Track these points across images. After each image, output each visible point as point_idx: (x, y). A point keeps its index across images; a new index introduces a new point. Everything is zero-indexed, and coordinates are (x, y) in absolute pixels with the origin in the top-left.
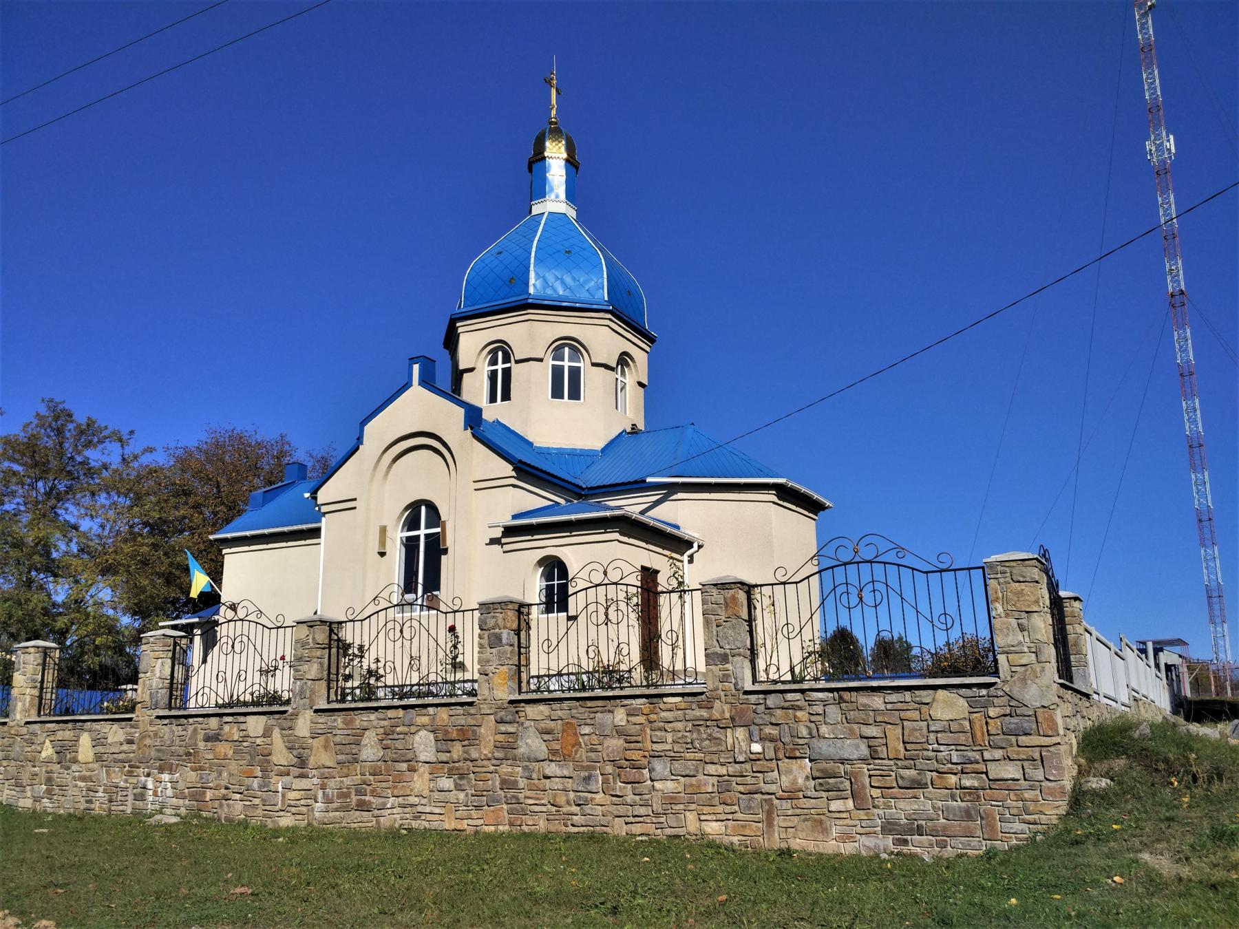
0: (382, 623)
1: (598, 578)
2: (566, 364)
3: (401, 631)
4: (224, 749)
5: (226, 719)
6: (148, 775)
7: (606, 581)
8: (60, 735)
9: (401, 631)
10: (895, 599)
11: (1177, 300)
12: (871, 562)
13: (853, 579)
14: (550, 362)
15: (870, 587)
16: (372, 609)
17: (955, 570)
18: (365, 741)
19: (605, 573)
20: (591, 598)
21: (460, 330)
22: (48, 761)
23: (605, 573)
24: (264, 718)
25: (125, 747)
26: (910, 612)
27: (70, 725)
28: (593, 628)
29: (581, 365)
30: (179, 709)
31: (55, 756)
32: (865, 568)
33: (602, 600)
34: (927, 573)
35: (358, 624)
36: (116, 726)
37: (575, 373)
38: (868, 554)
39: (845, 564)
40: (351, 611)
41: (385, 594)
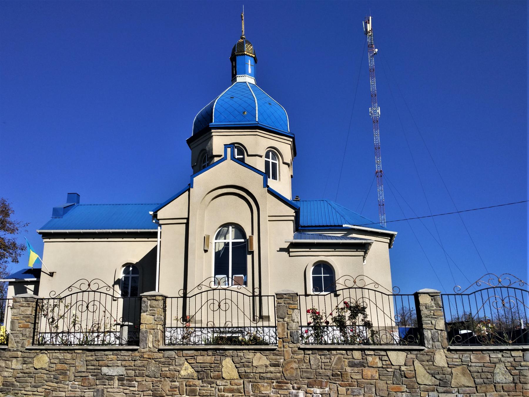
0: (204, 300)
1: (85, 287)
2: (271, 160)
3: (87, 307)
4: (368, 372)
5: (368, 352)
6: (299, 389)
7: (89, 290)
8: (200, 359)
9: (87, 307)
10: (235, 307)
11: (379, 174)
12: (362, 288)
13: (86, 299)
14: (264, 159)
15: (224, 301)
16: (67, 293)
17: (401, 295)
18: (497, 370)
19: (89, 285)
20: (80, 298)
21: (213, 134)
22: (189, 378)
23: (89, 285)
24: (404, 354)
25: (272, 369)
26: (380, 313)
27: (210, 353)
28: (211, 313)
29: (277, 162)
30: (350, 344)
31: (195, 374)
32: (92, 294)
33: (86, 299)
34: (388, 295)
35: (472, 297)
36: (258, 354)
37: (274, 165)
38: (94, 287)
39: (349, 288)
40: (53, 293)
41: (77, 285)
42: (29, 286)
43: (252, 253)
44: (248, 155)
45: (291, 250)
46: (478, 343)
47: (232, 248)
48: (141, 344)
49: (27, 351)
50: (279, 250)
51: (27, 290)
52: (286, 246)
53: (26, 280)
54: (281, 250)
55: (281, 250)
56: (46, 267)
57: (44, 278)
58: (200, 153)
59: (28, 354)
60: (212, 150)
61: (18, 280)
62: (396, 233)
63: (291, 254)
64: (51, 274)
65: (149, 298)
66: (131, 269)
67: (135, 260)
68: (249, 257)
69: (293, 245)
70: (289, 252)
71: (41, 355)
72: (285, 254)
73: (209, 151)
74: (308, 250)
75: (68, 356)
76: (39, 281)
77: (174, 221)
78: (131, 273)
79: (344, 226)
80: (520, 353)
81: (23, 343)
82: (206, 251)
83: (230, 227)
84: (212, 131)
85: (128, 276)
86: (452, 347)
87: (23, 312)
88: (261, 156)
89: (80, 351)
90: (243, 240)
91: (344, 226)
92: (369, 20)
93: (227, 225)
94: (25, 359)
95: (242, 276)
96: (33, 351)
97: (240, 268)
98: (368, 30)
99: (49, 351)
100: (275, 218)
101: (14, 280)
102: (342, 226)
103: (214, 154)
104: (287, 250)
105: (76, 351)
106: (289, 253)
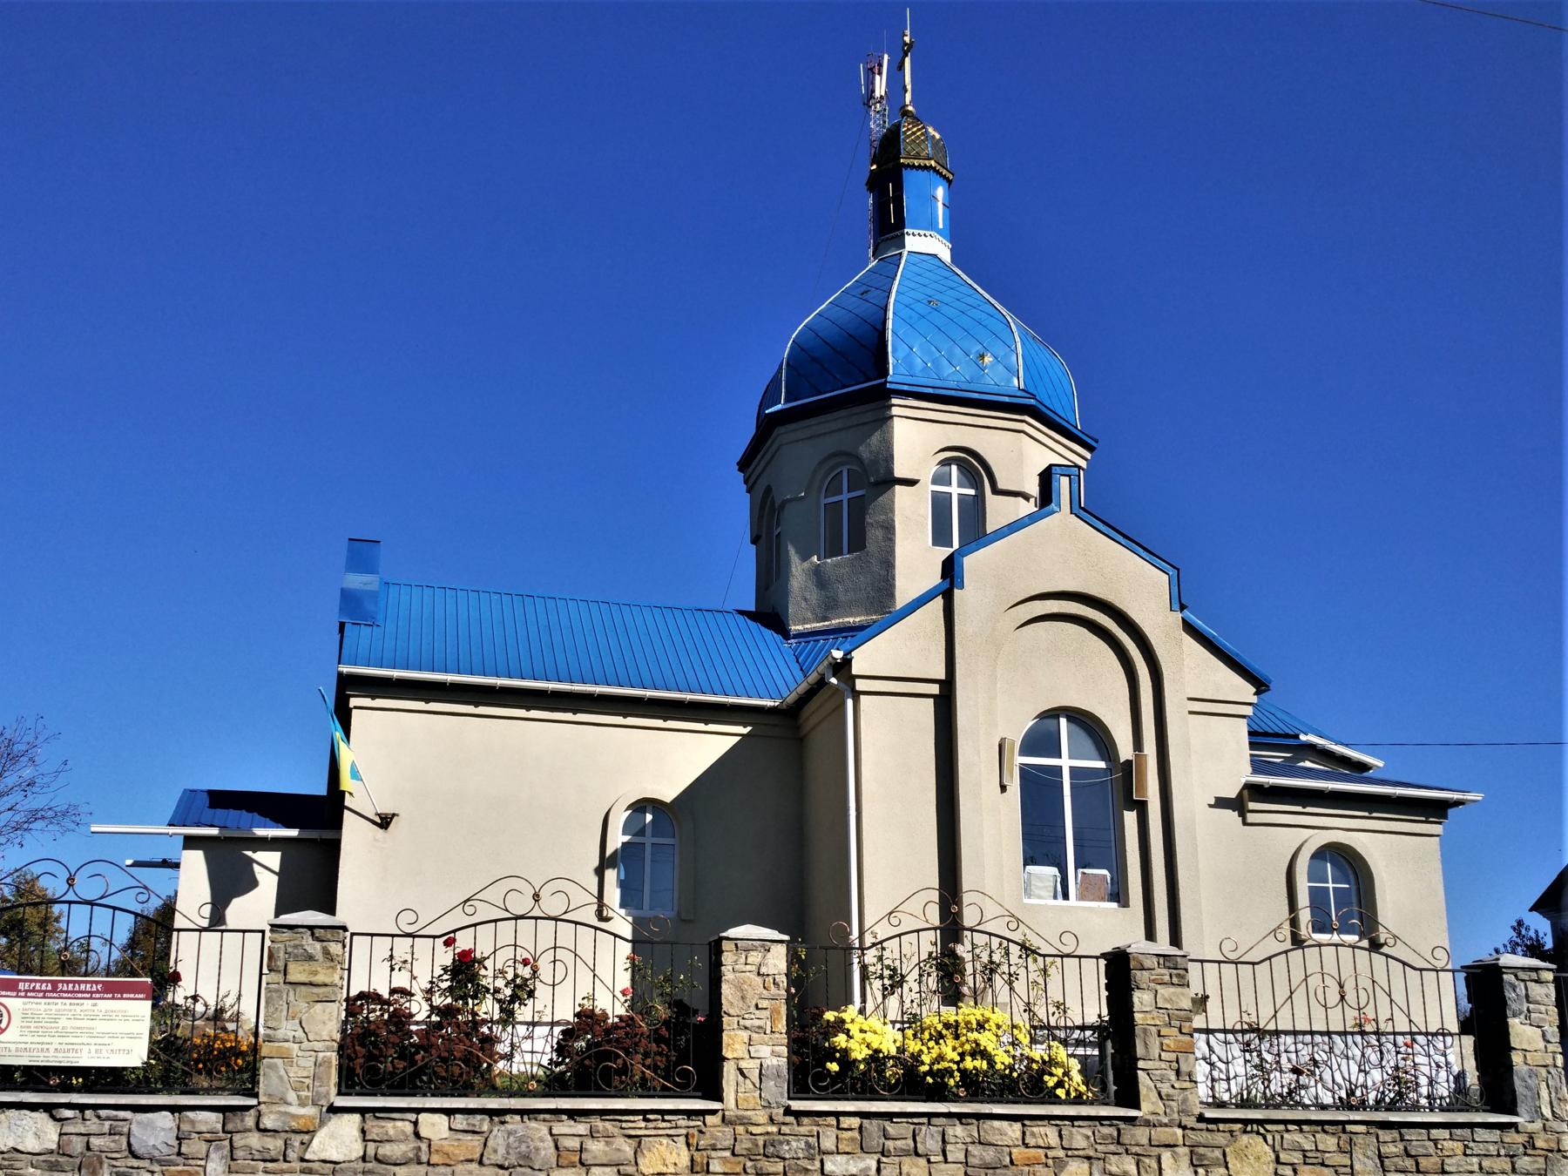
21: (895, 411)
42: (260, 856)
43: (1141, 808)
44: (996, 491)
45: (1252, 805)
46: (873, 1091)
47: (1072, 784)
48: (1521, 1108)
49: (1203, 1126)
50: (1212, 802)
51: (256, 868)
52: (1232, 793)
53: (260, 832)
54: (1221, 803)
55: (1221, 803)
56: (360, 796)
57: (354, 835)
58: (821, 463)
59: (1205, 1134)
60: (889, 459)
61: (228, 834)
62: (1380, 764)
63: (1251, 818)
64: (384, 822)
65: (1521, 975)
66: (649, 817)
67: (668, 792)
68: (1130, 818)
69: (1255, 792)
70: (1243, 812)
71: (1245, 1138)
72: (1232, 816)
73: (875, 462)
74: (1299, 809)
75: (1329, 1142)
76: (339, 841)
77: (900, 685)
78: (649, 831)
79: (1303, 737)
80: (214, 1119)
81: (1185, 1101)
82: (1003, 788)
83: (1063, 721)
84: (894, 401)
85: (639, 840)
86: (797, 1105)
87: (1166, 1000)
88: (1027, 497)
89: (1362, 1128)
90: (1102, 765)
91: (1303, 737)
92: (880, 65)
93: (1053, 714)
94: (1201, 1150)
95: (1105, 872)
96: (1221, 1127)
97: (1100, 848)
98: (877, 94)
99: (1268, 1127)
100: (1209, 707)
101: (214, 831)
102: (1297, 737)
103: (899, 472)
104: (1237, 804)
105: (103, 1113)
106: (1242, 815)
